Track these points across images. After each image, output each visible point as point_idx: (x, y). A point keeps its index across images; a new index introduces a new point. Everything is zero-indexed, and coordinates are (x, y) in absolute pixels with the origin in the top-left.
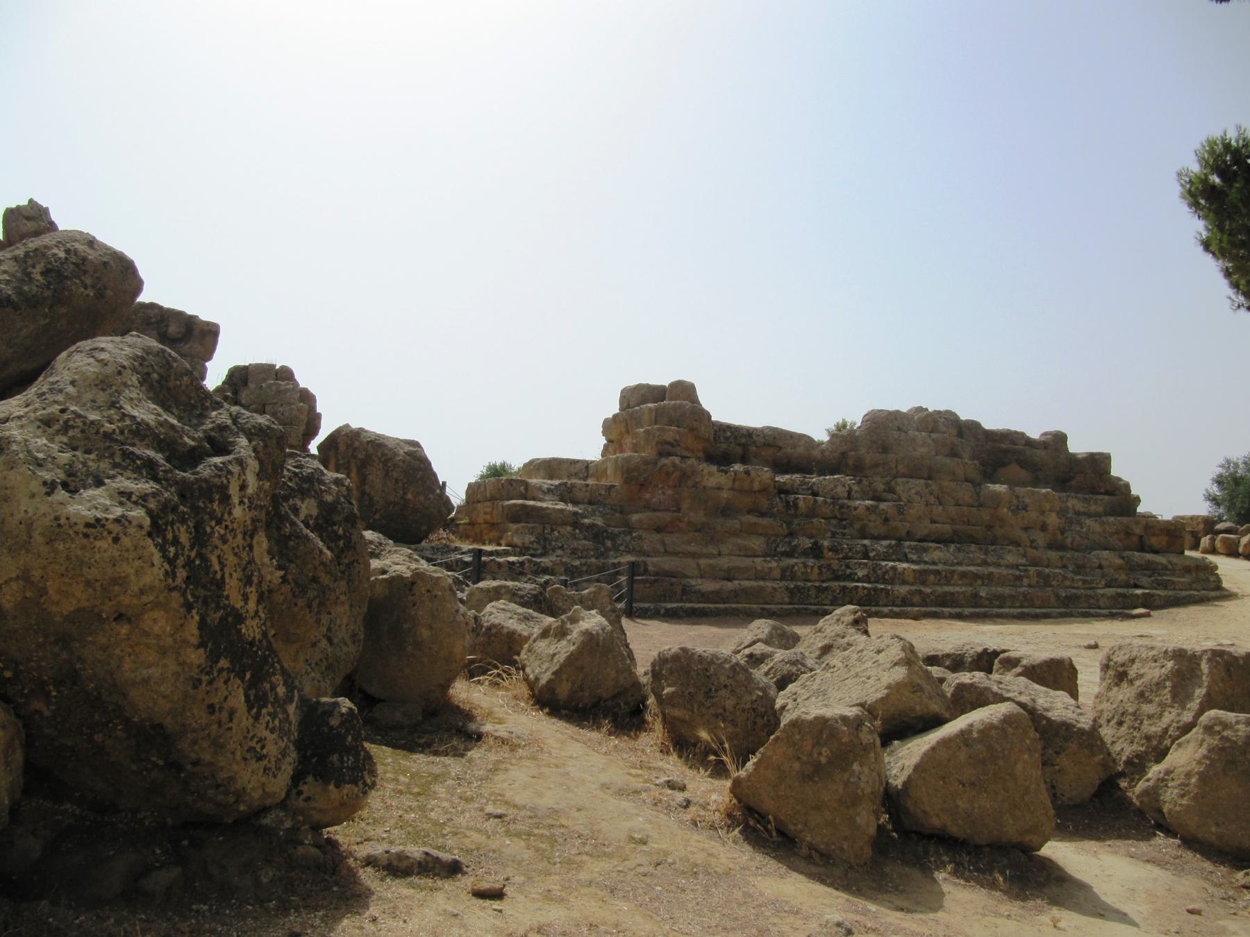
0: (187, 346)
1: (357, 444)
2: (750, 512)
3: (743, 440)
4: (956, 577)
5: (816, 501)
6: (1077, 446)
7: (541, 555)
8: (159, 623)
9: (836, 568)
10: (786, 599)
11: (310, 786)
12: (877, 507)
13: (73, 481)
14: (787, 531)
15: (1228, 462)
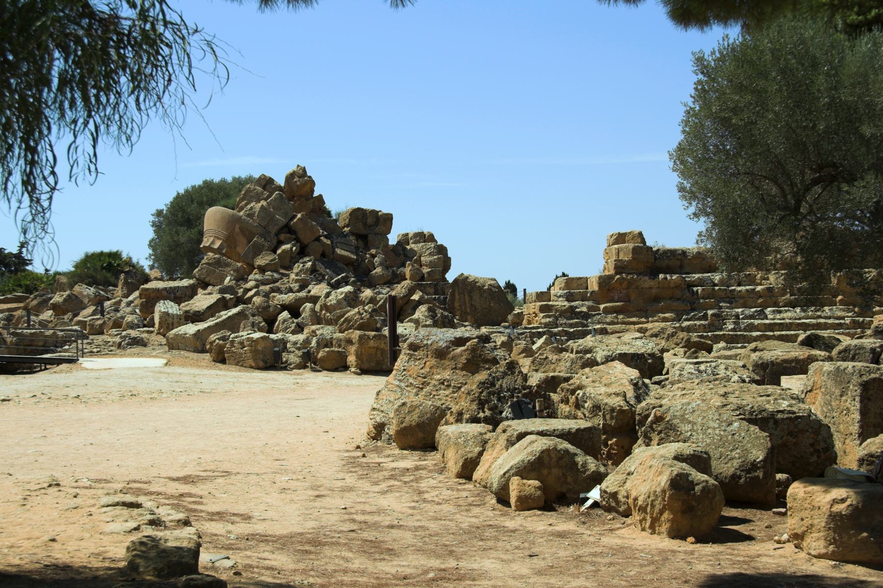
3: (679, 257)
4: (794, 326)
5: (714, 289)
12: (754, 289)
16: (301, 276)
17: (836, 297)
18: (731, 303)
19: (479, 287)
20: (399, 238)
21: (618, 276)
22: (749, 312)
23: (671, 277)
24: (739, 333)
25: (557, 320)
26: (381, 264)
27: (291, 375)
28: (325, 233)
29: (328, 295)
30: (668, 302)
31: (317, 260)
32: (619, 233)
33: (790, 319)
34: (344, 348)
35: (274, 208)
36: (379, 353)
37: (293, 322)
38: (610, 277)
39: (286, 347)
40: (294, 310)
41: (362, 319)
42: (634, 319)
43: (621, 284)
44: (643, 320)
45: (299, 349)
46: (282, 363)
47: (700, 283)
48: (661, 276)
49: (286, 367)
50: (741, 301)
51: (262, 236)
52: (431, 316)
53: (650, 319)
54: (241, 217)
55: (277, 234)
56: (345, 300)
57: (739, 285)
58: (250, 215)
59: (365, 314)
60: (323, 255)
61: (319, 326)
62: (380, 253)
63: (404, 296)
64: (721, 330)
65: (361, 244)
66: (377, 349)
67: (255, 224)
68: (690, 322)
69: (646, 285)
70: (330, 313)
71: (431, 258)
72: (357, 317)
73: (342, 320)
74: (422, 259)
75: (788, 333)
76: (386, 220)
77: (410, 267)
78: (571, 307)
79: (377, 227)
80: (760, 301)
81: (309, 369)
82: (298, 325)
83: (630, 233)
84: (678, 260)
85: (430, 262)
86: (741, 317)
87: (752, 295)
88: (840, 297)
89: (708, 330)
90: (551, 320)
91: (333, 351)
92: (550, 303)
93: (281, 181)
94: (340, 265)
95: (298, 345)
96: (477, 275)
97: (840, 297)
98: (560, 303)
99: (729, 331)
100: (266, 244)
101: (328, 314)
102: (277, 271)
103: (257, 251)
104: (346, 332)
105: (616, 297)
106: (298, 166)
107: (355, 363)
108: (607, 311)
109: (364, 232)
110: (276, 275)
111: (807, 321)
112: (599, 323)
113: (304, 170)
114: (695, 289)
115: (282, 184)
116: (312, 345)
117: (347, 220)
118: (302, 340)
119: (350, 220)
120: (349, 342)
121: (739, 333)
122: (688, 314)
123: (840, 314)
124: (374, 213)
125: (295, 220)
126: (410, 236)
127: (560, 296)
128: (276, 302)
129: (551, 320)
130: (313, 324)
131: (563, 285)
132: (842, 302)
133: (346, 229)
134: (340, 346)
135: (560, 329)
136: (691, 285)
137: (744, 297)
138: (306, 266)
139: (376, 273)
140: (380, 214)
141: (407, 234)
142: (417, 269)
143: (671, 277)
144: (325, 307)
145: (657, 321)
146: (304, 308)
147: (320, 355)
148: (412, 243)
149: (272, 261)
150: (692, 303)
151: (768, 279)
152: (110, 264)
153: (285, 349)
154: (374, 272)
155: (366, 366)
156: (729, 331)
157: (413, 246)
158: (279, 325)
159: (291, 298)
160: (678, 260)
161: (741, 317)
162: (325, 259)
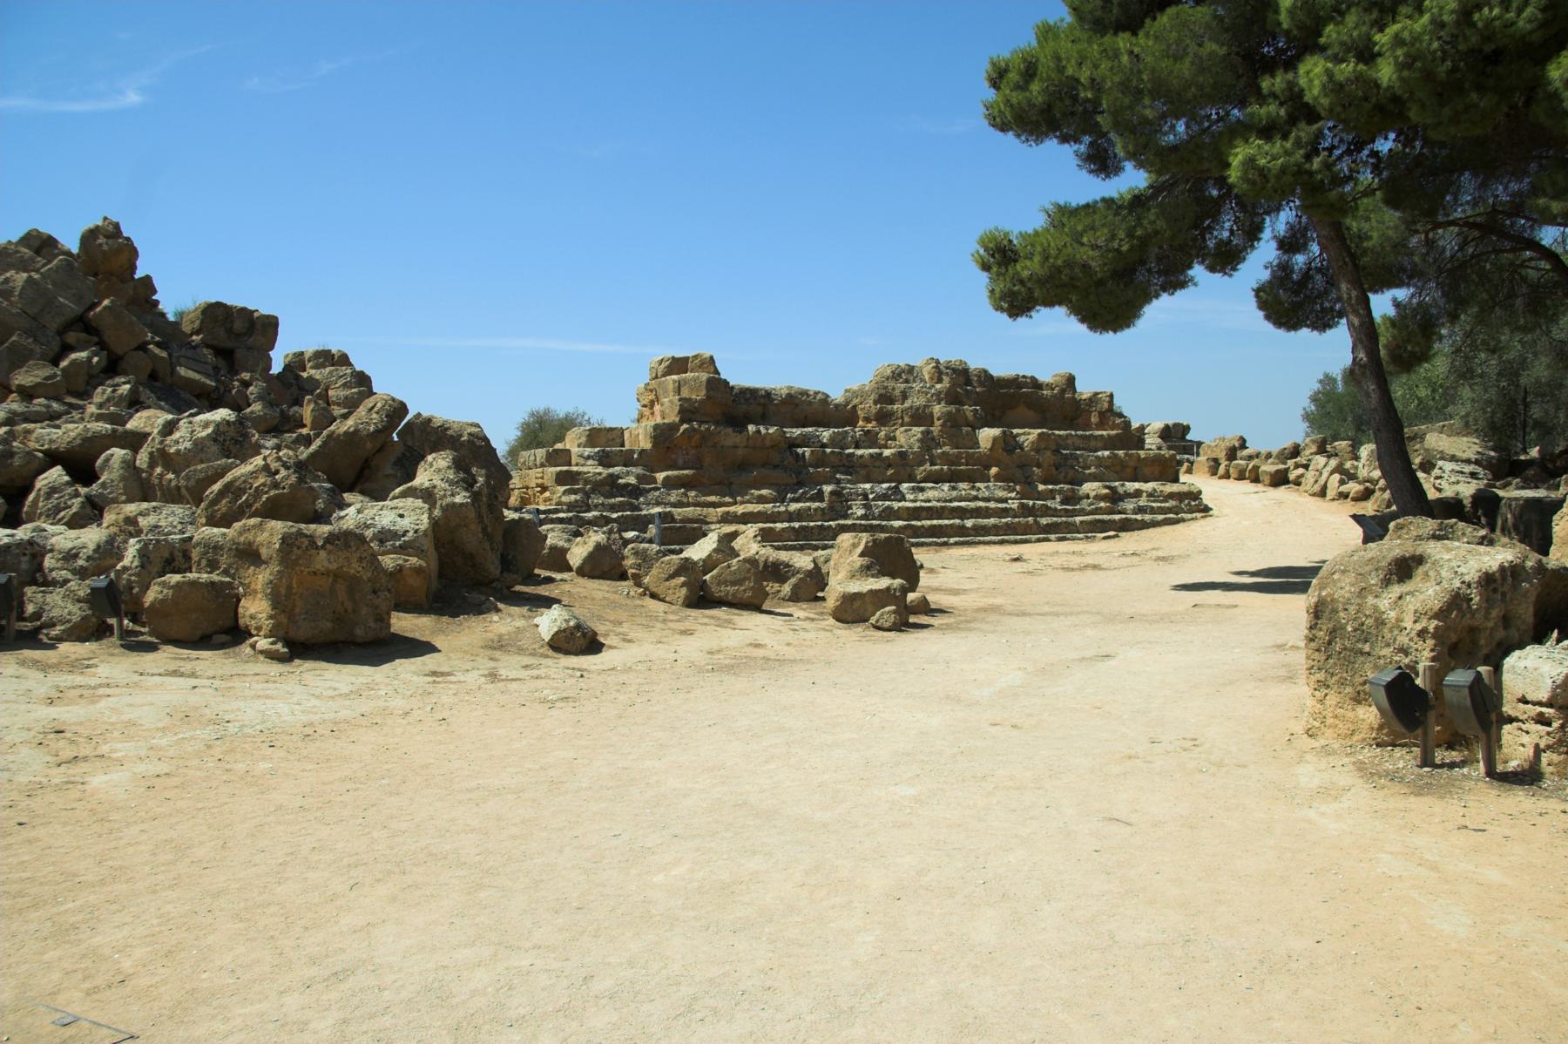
0: (251, 339)
1: (429, 429)
2: (764, 465)
3: (762, 401)
4: (947, 512)
5: (825, 452)
6: (1084, 389)
7: (585, 512)
8: (473, 527)
9: (839, 509)
10: (793, 537)
11: (505, 575)
12: (881, 454)
13: (854, 546)
14: (795, 481)
15: (1327, 376)
16: (108, 409)
17: (988, 468)
19: (452, 436)
20: (288, 359)
21: (685, 426)
23: (767, 429)
24: (874, 522)
25: (589, 497)
26: (260, 398)
27: (44, 668)
28: (157, 339)
29: (169, 428)
30: (763, 470)
31: (141, 384)
32: (673, 357)
33: (938, 501)
34: (226, 573)
35: (54, 284)
36: (341, 588)
37: (77, 495)
38: (672, 428)
39: (40, 568)
40: (81, 465)
41: (276, 485)
42: (713, 498)
43: (690, 438)
44: (728, 499)
45: (82, 574)
46: (21, 618)
47: (805, 441)
48: (751, 428)
49: (38, 630)
50: (863, 472)
51: (28, 332)
52: (463, 480)
53: (738, 498)
55: (61, 332)
56: (215, 440)
57: (857, 447)
59: (283, 472)
60: (153, 376)
61: (145, 505)
62: (258, 379)
63: (378, 432)
64: (846, 517)
65: (221, 363)
66: (337, 576)
67: (14, 311)
68: (801, 505)
69: (729, 442)
70: (177, 473)
71: (348, 392)
72: (261, 480)
73: (217, 487)
74: (331, 393)
75: (940, 522)
76: (269, 326)
77: (312, 406)
78: (611, 475)
79: (251, 336)
80: (890, 472)
81: (115, 639)
82: (89, 500)
83: (696, 357)
84: (759, 404)
85: (346, 398)
86: (871, 496)
87: (878, 464)
88: (994, 470)
89: (827, 518)
90: (578, 497)
91: (194, 584)
92: (575, 469)
93: (71, 242)
94: (186, 395)
95: (81, 562)
96: (445, 418)
97: (994, 470)
98: (591, 469)
99: (858, 518)
100: (38, 349)
101: (171, 476)
102: (58, 399)
103: (19, 359)
104: (237, 525)
105: (680, 462)
106: (105, 219)
107: (267, 624)
108: (669, 484)
109: (228, 344)
111: (963, 504)
112: (658, 504)
113: (117, 226)
114: (800, 451)
115: (75, 250)
116: (126, 562)
117: (198, 322)
118: (92, 546)
119: (202, 322)
120: (249, 555)
121: (874, 522)
122: (795, 492)
123: (1001, 494)
124: (245, 313)
125: (98, 309)
126: (307, 356)
127: (588, 458)
128: (33, 445)
129: (578, 497)
130: (130, 500)
131: (584, 439)
132: (998, 478)
133: (194, 337)
134: (213, 566)
135: (595, 513)
136: (793, 444)
137: (866, 466)
138: (120, 392)
139: (252, 412)
140: (256, 315)
141: (302, 354)
142: (323, 409)
143: (767, 429)
144: (162, 457)
145: (749, 502)
146: (107, 460)
147: (151, 596)
148: (312, 368)
149: (47, 378)
150: (798, 474)
153: (37, 576)
154: (248, 410)
155: (303, 632)
156: (858, 518)
157: (313, 372)
158: (36, 501)
159: (72, 434)
160: (759, 404)
161: (871, 496)
162: (157, 384)
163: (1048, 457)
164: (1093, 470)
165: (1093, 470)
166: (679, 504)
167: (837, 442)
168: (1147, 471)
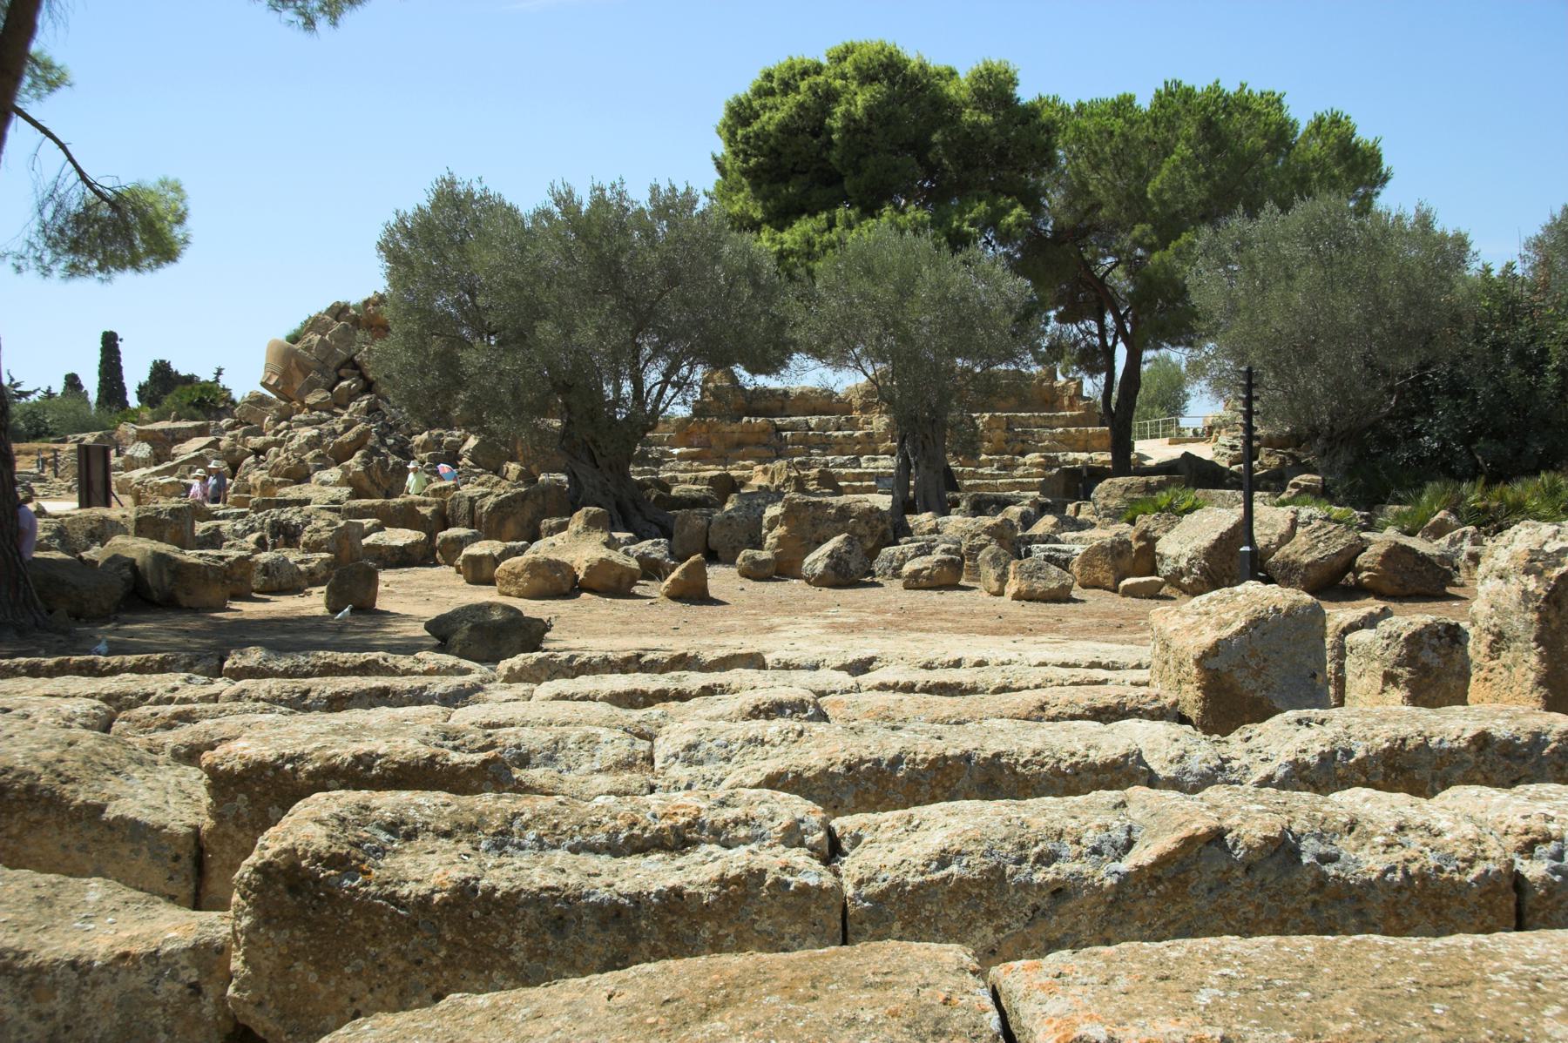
18: (824, 449)
22: (840, 459)
47: (793, 427)
48: (745, 419)
50: (837, 448)
51: (319, 371)
54: (296, 351)
55: (337, 370)
58: (308, 349)
69: (728, 429)
100: (323, 381)
103: (311, 387)
110: (325, 415)
136: (779, 429)
151: (871, 423)
152: (201, 400)
163: (999, 434)
164: (1046, 443)
165: (1046, 443)
166: (685, 471)
167: (822, 427)
168: (1095, 443)
